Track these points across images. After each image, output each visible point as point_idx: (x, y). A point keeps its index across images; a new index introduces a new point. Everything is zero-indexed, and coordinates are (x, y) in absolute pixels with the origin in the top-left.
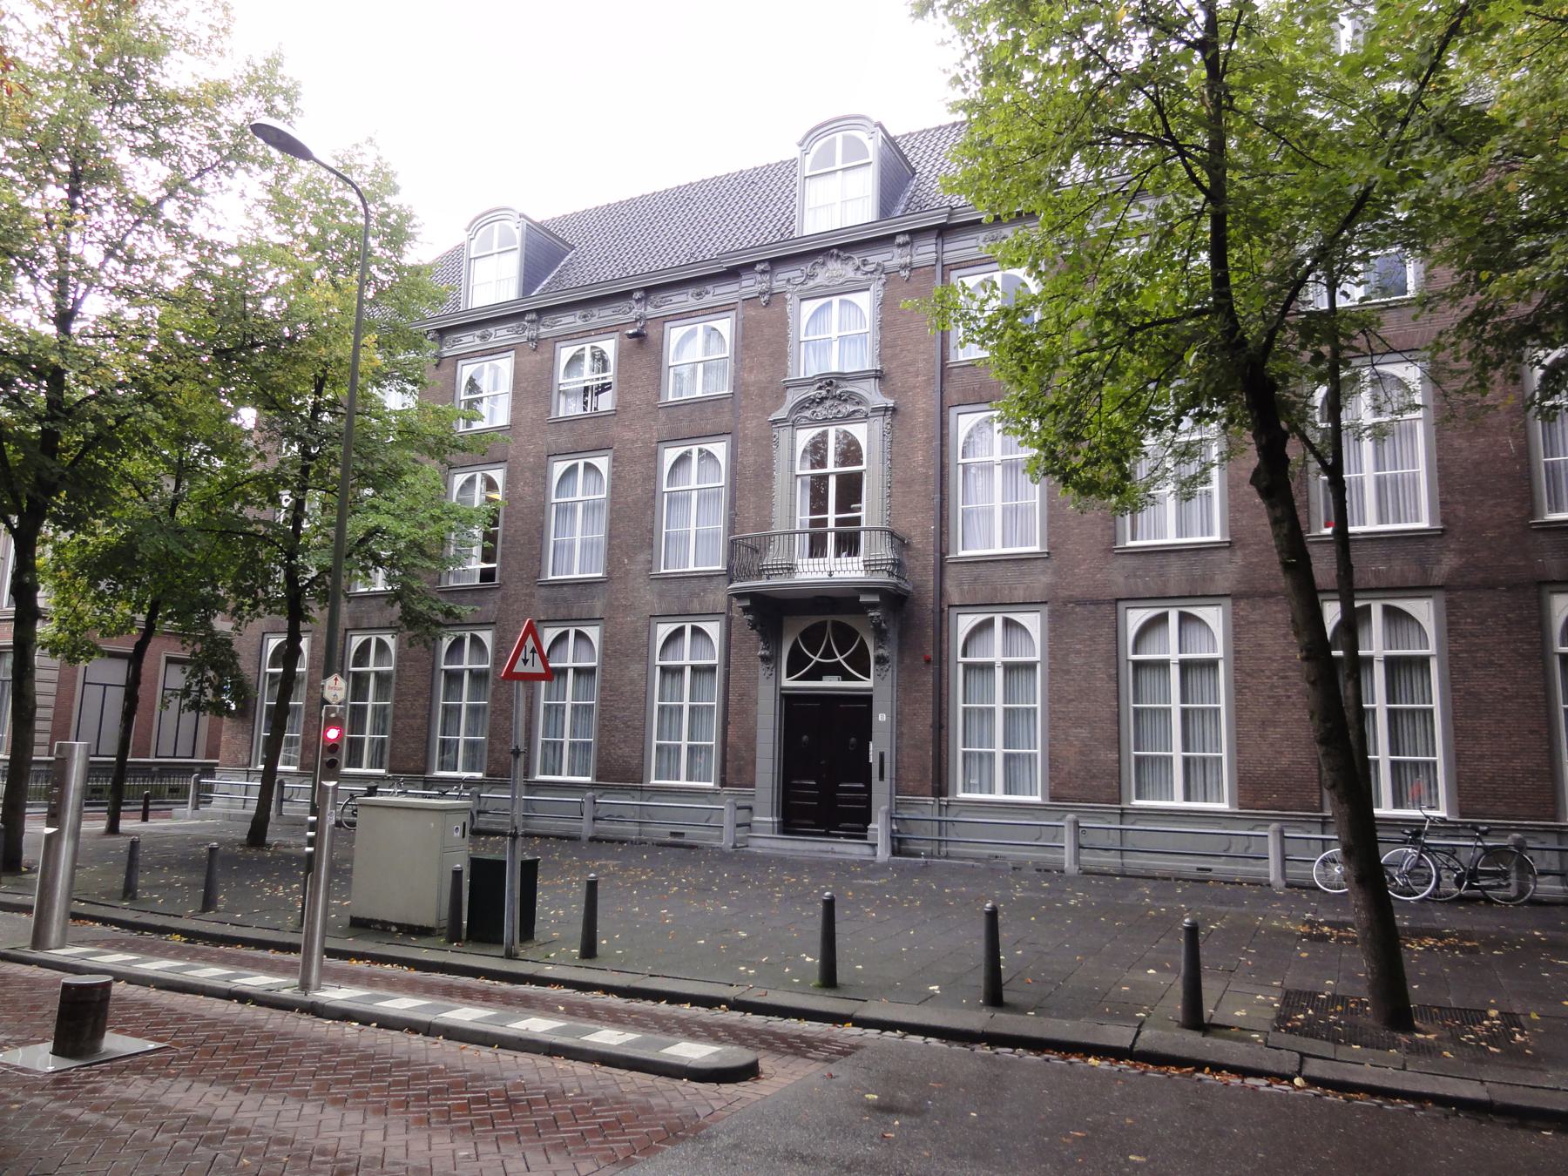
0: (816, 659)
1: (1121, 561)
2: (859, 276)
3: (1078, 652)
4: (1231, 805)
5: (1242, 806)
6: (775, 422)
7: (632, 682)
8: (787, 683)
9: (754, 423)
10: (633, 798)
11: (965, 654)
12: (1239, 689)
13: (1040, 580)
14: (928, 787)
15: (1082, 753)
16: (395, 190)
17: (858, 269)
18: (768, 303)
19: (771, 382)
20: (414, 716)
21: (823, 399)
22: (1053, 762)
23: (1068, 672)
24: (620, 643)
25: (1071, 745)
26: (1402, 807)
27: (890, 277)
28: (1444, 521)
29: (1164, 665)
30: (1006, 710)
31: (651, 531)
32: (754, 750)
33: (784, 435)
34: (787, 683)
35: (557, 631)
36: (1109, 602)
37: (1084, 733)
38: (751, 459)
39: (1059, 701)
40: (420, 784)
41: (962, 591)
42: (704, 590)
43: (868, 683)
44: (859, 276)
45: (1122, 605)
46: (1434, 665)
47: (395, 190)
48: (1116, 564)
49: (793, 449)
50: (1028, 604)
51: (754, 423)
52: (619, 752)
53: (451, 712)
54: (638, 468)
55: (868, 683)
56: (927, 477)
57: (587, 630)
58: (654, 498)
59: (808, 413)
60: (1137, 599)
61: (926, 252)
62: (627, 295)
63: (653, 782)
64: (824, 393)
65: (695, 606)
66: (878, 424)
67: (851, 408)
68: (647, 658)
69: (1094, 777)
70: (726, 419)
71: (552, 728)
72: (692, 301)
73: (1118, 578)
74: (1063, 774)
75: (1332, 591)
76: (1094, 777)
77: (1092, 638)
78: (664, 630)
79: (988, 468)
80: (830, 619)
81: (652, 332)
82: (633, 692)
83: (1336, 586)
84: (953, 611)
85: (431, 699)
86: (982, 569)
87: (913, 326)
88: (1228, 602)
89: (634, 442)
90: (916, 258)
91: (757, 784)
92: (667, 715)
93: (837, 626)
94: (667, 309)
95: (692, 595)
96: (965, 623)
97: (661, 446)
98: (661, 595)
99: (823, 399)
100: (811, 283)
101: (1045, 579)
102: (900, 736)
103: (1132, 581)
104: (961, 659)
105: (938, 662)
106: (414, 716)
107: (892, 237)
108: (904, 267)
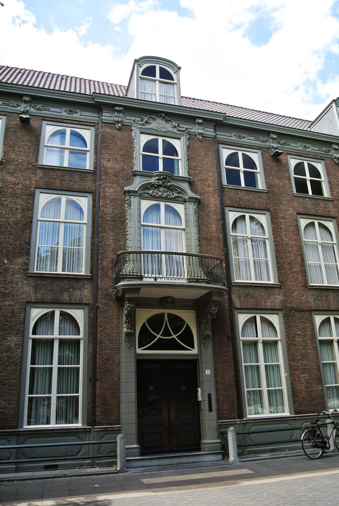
0: (159, 336)
2: (175, 130)
3: (299, 335)
5: (296, 413)
6: (129, 192)
7: (9, 349)
8: (139, 351)
9: (112, 190)
10: (9, 442)
11: (34, 333)
13: (278, 299)
14: (235, 414)
15: (307, 387)
17: (175, 127)
18: (120, 129)
19: (123, 170)
21: (159, 186)
23: (296, 345)
25: (301, 383)
26: (30, 425)
27: (191, 137)
28: (91, 272)
29: (51, 342)
30: (59, 368)
31: (29, 244)
33: (134, 200)
34: (139, 351)
35: (324, 317)
37: (306, 376)
38: (110, 210)
39: (294, 360)
41: (240, 301)
42: (73, 288)
43: (195, 351)
45: (313, 313)
48: (309, 293)
49: (140, 210)
50: (273, 310)
51: (112, 190)
53: (68, 376)
54: (19, 201)
55: (195, 351)
56: (219, 238)
58: (31, 222)
60: (319, 311)
61: (210, 132)
62: (268, 133)
63: (26, 427)
64: (161, 183)
65: (65, 297)
67: (176, 195)
68: (23, 333)
69: (314, 399)
70: (89, 184)
72: (64, 114)
73: (310, 300)
74: (300, 399)
75: (335, 311)
76: (314, 399)
77: (304, 328)
78: (36, 313)
79: (245, 240)
80: (166, 311)
81: (34, 123)
82: (9, 358)
83: (338, 309)
84: (236, 312)
86: (250, 291)
87: (204, 163)
89: (15, 184)
90: (124, 120)
91: (123, 421)
92: (250, 371)
93: (173, 318)
94: (44, 113)
95: (62, 290)
96: (242, 318)
97: (37, 191)
98: (36, 288)
99: (159, 186)
100: (148, 126)
102: (217, 383)
103: (316, 302)
104: (31, 336)
105: (233, 337)
107: (195, 118)
108: (200, 134)
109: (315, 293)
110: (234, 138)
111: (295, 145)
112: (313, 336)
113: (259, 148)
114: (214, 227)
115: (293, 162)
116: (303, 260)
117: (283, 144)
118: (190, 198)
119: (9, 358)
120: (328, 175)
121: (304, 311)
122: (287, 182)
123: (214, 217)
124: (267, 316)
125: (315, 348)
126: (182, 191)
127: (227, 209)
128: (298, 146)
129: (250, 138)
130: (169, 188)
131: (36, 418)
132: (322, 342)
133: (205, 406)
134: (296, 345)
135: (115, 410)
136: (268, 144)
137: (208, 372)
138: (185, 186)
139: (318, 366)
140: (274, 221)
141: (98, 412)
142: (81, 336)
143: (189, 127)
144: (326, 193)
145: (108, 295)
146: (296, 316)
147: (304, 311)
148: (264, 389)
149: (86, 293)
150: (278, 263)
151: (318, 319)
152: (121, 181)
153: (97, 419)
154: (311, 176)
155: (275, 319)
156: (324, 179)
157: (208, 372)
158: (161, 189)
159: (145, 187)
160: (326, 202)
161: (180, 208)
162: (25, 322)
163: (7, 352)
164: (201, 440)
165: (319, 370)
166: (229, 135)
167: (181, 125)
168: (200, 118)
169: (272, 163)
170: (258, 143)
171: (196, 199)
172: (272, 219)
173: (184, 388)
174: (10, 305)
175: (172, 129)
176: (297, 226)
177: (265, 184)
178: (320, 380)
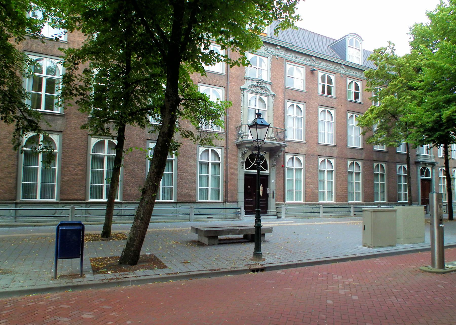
0: (253, 164)
1: (319, 147)
2: (266, 52)
4: (363, 201)
12: (337, 177)
13: (304, 149)
16: (422, 24)
19: (240, 75)
20: (76, 175)
22: (306, 193)
24: (185, 152)
32: (237, 190)
36: (371, 161)
37: (312, 186)
38: (234, 98)
40: (85, 205)
43: (267, 172)
44: (266, 52)
46: (385, 176)
47: (422, 24)
50: (301, 154)
51: (234, 87)
52: (187, 191)
55: (267, 172)
57: (331, 160)
59: (253, 89)
60: (321, 156)
63: (199, 201)
66: (271, 99)
67: (265, 92)
68: (195, 158)
71: (169, 183)
82: (191, 170)
85: (86, 167)
88: (335, 158)
96: (288, 157)
97: (199, 84)
101: (305, 149)
102: (276, 186)
106: (76, 175)
107: (276, 45)
109: (321, 147)
110: (294, 58)
111: (323, 64)
112: (317, 168)
113: (305, 65)
114: (280, 111)
115: (320, 74)
116: (318, 130)
117: (317, 63)
118: (271, 94)
119: (191, 170)
120: (336, 83)
121: (315, 156)
122: (316, 86)
123: (281, 105)
124: (298, 157)
125: (317, 174)
126: (267, 90)
127: (286, 100)
128: (323, 64)
129: (301, 59)
130: (261, 88)
131: (44, 196)
132: (320, 171)
133: (271, 196)
134: (309, 172)
135: (235, 195)
136: (309, 63)
137: (273, 181)
138: (269, 87)
139: (318, 182)
140: (307, 108)
141: (229, 196)
142: (220, 162)
143: (273, 50)
144: (333, 94)
145: (233, 143)
146: (311, 157)
147: (315, 156)
148: (294, 190)
149: (223, 143)
150: (306, 131)
151: (320, 160)
152: (239, 82)
153: (228, 199)
154: (328, 83)
155: (302, 159)
156: (333, 85)
157: (273, 181)
158: (258, 88)
159: (251, 87)
160: (333, 99)
161: (265, 99)
162: (196, 154)
163: (190, 167)
164: (267, 209)
165: (318, 184)
166: (291, 56)
167: (269, 49)
168: (279, 46)
169: (309, 74)
170: (305, 62)
171: (274, 95)
172: (306, 107)
173: (249, 187)
174: (190, 145)
175: (264, 51)
176: (317, 112)
177: (305, 87)
178: (317, 188)
